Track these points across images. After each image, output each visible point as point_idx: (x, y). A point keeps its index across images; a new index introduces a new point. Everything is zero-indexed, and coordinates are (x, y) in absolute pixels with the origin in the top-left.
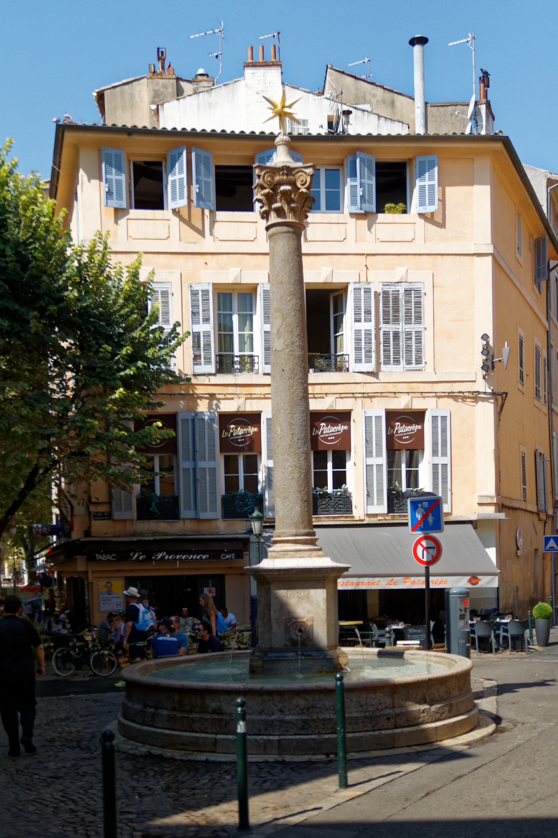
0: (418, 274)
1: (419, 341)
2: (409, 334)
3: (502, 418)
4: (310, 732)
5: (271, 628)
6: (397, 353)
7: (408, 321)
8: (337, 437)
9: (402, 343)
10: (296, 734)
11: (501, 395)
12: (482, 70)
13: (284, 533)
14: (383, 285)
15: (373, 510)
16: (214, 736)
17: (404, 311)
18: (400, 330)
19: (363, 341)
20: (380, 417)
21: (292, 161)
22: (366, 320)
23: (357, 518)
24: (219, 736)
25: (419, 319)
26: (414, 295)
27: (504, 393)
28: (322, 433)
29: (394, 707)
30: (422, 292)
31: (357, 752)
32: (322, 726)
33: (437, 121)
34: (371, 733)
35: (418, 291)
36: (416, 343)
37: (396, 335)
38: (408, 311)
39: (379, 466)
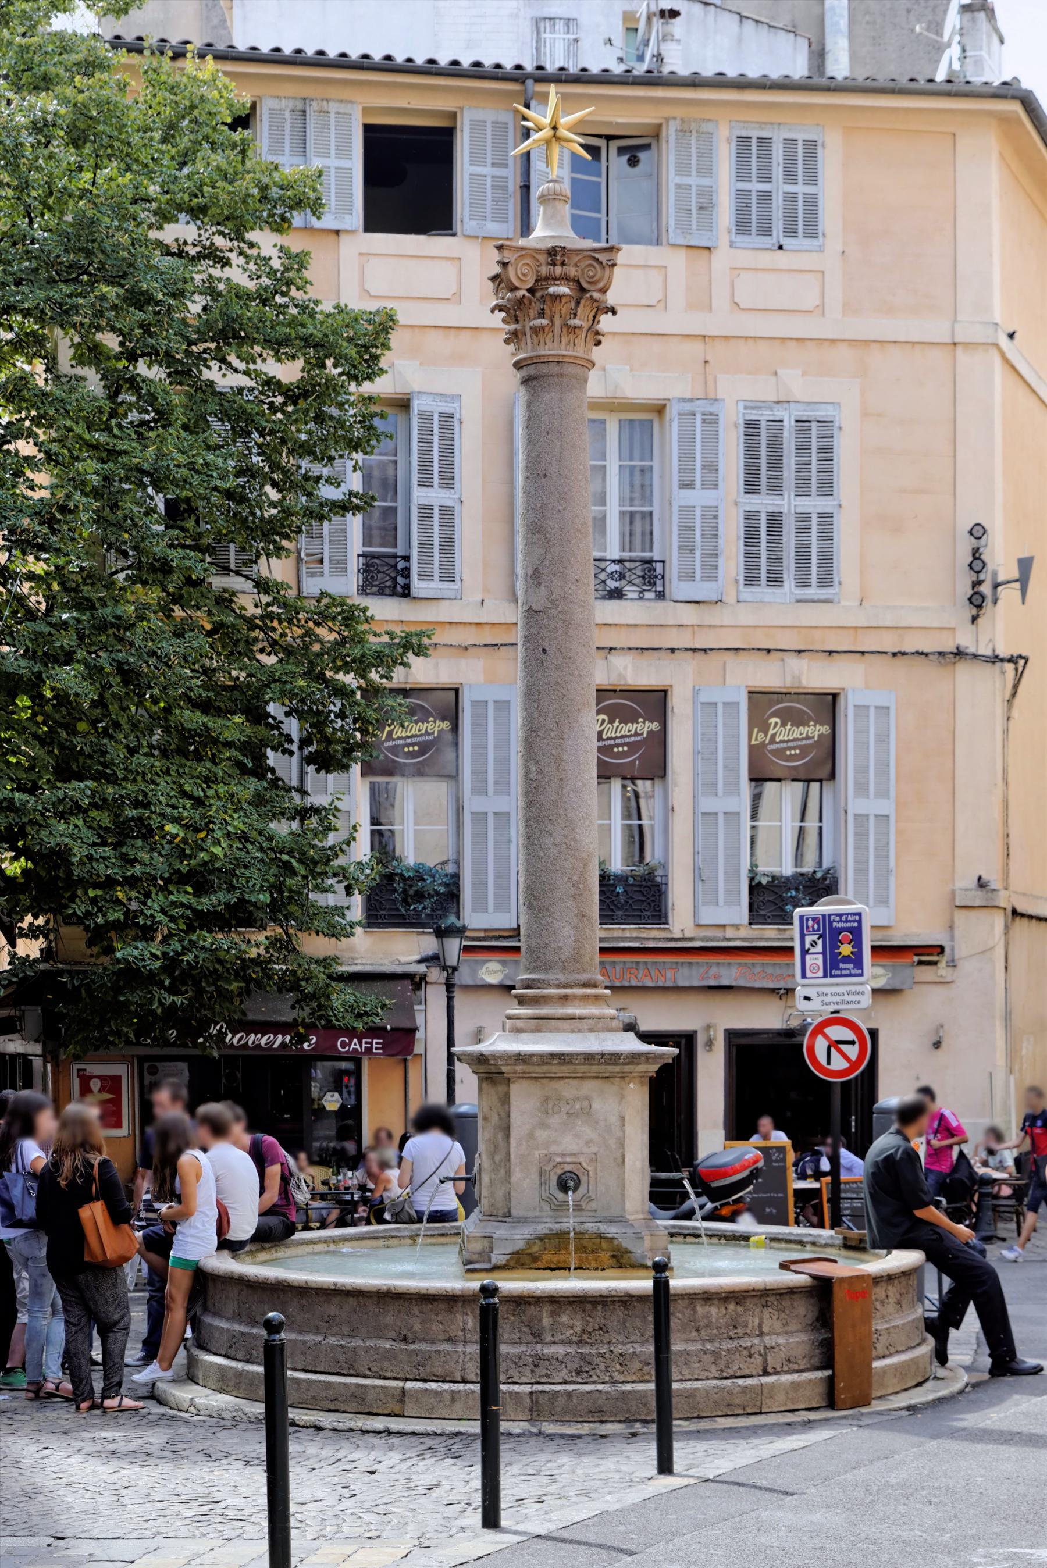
1: (827, 535)
2: (803, 519)
3: (1015, 713)
4: (594, 1378)
5: (508, 1173)
7: (803, 489)
8: (633, 747)
9: (789, 538)
10: (565, 1383)
11: (1011, 660)
13: (539, 980)
14: (746, 408)
15: (709, 916)
16: (400, 1384)
17: (793, 467)
18: (785, 510)
19: (698, 533)
20: (734, 705)
21: (573, 235)
22: (704, 486)
23: (677, 934)
24: (409, 1385)
25: (827, 487)
26: (818, 434)
27: (1021, 657)
29: (761, 1334)
30: (837, 424)
31: (687, 1419)
32: (618, 1366)
33: (875, 23)
34: (715, 1382)
35: (825, 423)
36: (821, 539)
37: (775, 521)
38: (803, 467)
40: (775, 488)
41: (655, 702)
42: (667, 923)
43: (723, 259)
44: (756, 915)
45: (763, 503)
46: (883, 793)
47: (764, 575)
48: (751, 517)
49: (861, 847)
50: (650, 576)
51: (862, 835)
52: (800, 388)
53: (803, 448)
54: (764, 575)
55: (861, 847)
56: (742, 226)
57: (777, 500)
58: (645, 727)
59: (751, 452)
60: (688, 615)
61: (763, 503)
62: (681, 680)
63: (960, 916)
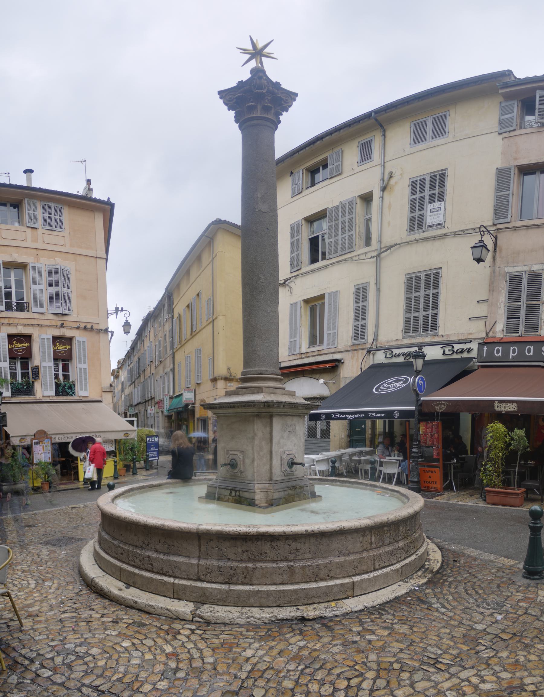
0: (69, 265)
6: (58, 302)
12: (89, 182)
15: (46, 393)
28: (15, 347)
37: (57, 293)
39: (50, 367)
40: (57, 285)
41: (28, 338)
42: (530, 479)
43: (40, 231)
44: (57, 393)
45: (54, 289)
46: (85, 363)
47: (55, 306)
48: (51, 292)
49: (81, 376)
50: (21, 307)
51: (81, 373)
52: (60, 262)
53: (64, 276)
54: (55, 306)
55: (81, 376)
56: (45, 224)
57: (58, 288)
58: (27, 345)
59: (50, 277)
60: (37, 316)
61: (54, 289)
62: (36, 333)
63: (104, 394)
